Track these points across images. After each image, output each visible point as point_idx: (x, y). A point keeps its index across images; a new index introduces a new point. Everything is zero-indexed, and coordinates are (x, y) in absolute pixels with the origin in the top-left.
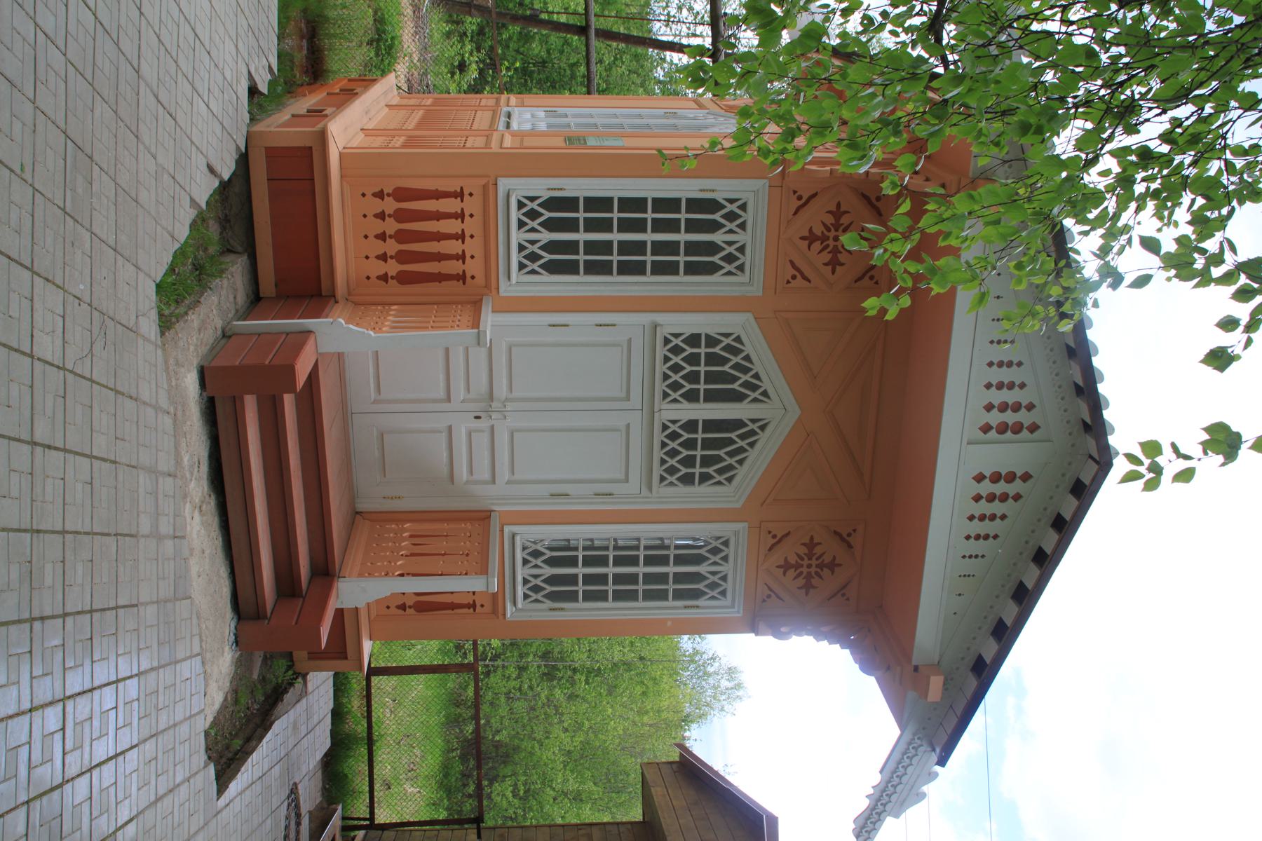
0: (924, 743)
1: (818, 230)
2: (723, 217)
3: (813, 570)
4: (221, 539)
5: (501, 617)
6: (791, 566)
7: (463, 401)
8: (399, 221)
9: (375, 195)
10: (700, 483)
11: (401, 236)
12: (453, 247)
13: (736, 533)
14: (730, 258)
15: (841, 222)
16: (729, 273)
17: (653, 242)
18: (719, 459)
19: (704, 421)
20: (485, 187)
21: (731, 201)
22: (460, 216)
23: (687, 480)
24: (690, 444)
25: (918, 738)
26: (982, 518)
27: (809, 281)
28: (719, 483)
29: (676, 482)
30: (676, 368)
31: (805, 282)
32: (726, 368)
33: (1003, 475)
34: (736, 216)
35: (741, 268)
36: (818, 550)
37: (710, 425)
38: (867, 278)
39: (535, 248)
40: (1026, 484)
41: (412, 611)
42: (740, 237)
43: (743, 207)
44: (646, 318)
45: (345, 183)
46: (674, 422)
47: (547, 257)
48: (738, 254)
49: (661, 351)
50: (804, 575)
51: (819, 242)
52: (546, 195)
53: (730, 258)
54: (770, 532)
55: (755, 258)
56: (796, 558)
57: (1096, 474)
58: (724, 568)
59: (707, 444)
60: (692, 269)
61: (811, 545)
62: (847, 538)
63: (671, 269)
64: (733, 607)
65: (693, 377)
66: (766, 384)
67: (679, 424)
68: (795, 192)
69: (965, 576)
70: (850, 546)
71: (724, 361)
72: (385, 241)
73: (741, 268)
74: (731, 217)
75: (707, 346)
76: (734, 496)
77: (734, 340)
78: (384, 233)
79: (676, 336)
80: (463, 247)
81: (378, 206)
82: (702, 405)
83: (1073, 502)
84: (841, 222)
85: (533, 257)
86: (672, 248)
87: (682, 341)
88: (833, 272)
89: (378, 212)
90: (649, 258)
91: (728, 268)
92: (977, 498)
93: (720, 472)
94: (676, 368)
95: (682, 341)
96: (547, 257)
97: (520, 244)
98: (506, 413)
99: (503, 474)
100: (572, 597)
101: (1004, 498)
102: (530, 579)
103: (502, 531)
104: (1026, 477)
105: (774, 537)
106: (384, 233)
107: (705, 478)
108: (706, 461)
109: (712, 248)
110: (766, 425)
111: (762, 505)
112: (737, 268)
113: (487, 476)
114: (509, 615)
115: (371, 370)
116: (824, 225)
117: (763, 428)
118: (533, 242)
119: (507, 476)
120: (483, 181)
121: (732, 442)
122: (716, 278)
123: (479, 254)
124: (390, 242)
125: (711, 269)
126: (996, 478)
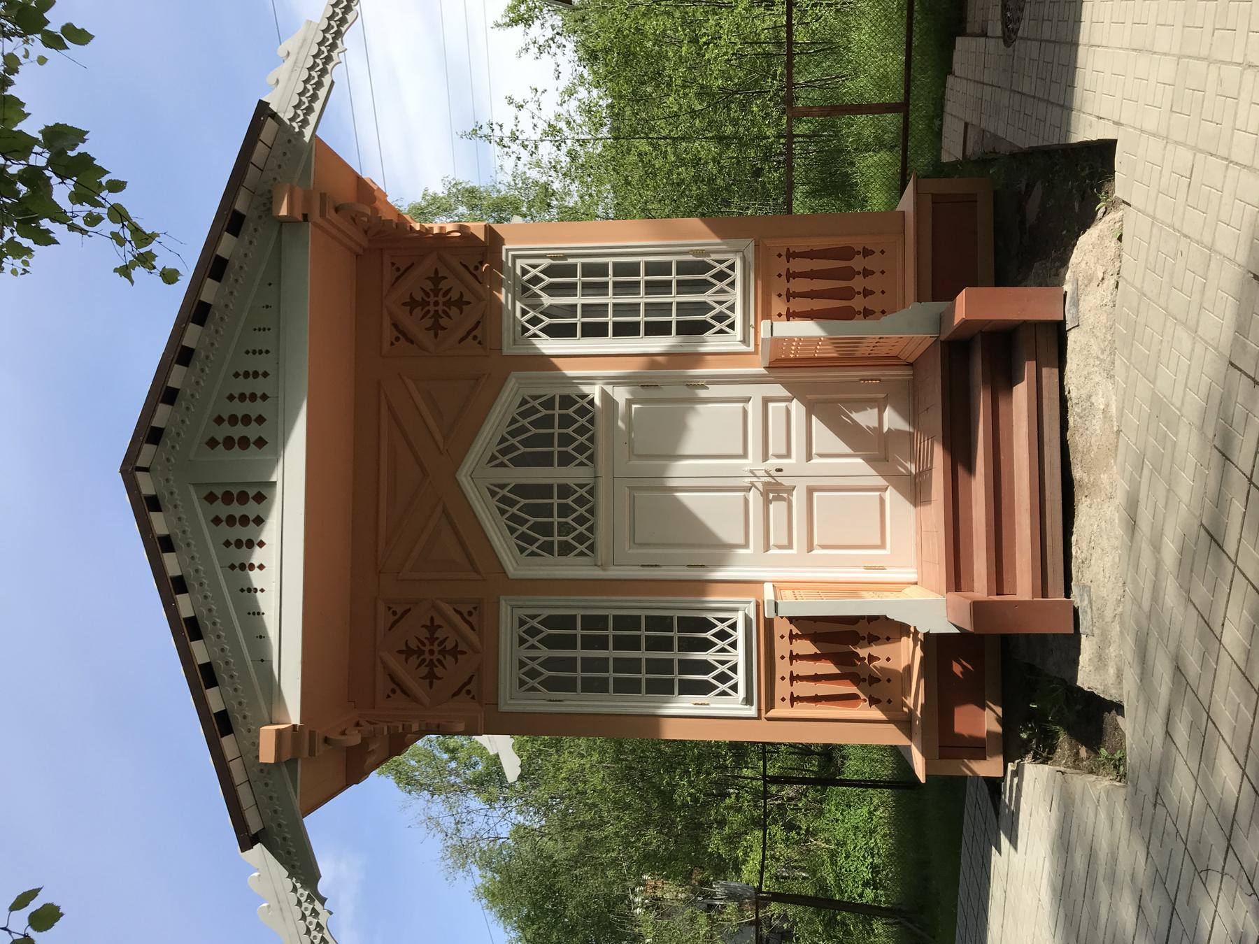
0: (288, 122)
3: (432, 300)
4: (1076, 499)
10: (553, 398)
15: (427, 669)
16: (533, 617)
17: (615, 659)
19: (552, 465)
21: (533, 689)
26: (253, 397)
27: (455, 610)
28: (535, 398)
29: (538, 644)
30: (581, 520)
31: (460, 609)
32: (532, 520)
33: (238, 523)
34: (727, 636)
37: (545, 460)
38: (470, 619)
39: (720, 644)
40: (211, 436)
42: (524, 653)
43: (522, 683)
48: (525, 636)
50: (441, 658)
51: (453, 299)
53: (533, 632)
57: (182, 336)
59: (548, 441)
60: (569, 621)
62: (399, 335)
63: (590, 622)
67: (577, 462)
69: (264, 329)
74: (533, 674)
75: (552, 542)
80: (789, 305)
82: (555, 482)
83: (223, 250)
84: (427, 669)
92: (260, 420)
93: (534, 410)
95: (577, 458)
99: (753, 409)
100: (683, 268)
101: (233, 420)
104: (212, 443)
105: (475, 338)
107: (549, 404)
108: (547, 422)
109: (550, 642)
110: (490, 461)
112: (526, 623)
116: (419, 666)
117: (493, 458)
119: (750, 406)
120: (772, 713)
121: (525, 443)
122: (546, 613)
124: (859, 268)
125: (550, 622)
126: (244, 443)
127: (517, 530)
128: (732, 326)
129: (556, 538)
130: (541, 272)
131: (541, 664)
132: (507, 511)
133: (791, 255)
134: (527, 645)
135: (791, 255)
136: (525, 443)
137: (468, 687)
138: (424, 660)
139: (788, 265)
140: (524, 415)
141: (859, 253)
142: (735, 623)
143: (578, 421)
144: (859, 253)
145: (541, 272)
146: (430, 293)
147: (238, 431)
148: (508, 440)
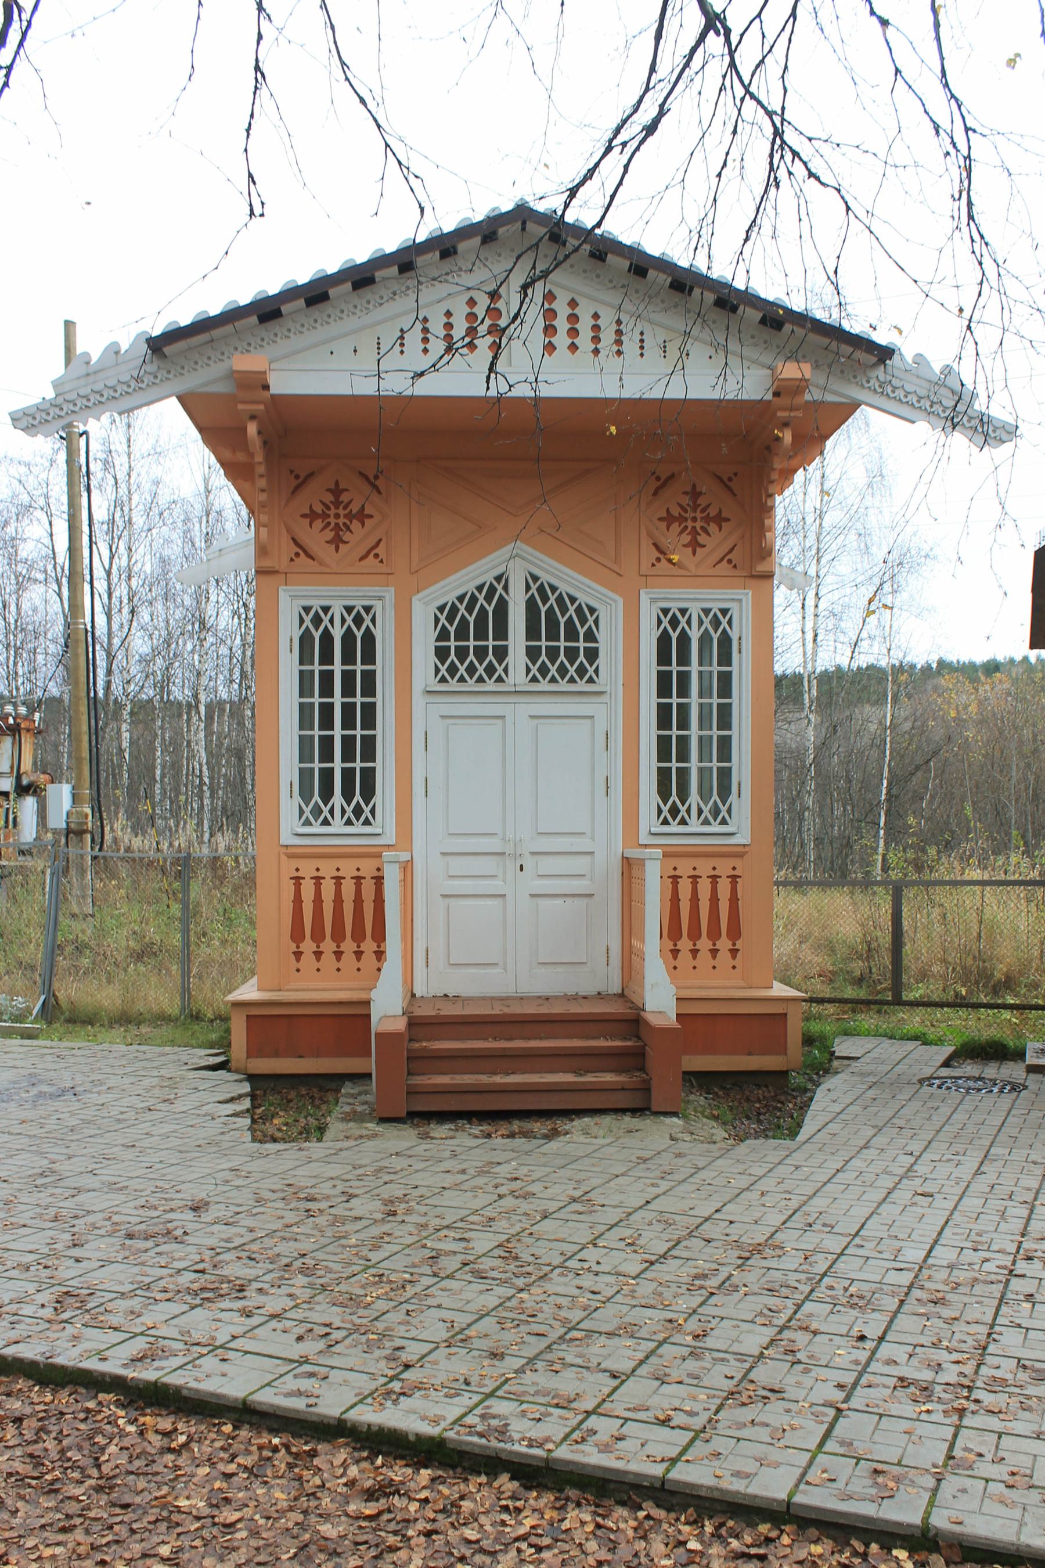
1: (329, 534)
2: (359, 629)
3: (341, 512)
5: (747, 849)
6: (337, 535)
7: (505, 881)
8: (324, 938)
9: (298, 960)
10: (597, 642)
11: (338, 936)
12: (704, 888)
13: (653, 600)
14: (358, 621)
15: (677, 515)
18: (570, 622)
20: (290, 856)
21: (302, 621)
22: (695, 879)
23: (592, 655)
24: (553, 654)
25: (868, 382)
27: (380, 540)
30: (471, 670)
35: (368, 609)
36: (676, 511)
37: (532, 632)
39: (349, 810)
41: (739, 945)
42: (337, 611)
43: (307, 609)
44: (418, 700)
45: (287, 987)
46: (528, 670)
47: (357, 798)
49: (453, 685)
50: (706, 525)
52: (297, 799)
53: (358, 621)
54: (653, 565)
55: (358, 595)
56: (327, 530)
58: (695, 611)
59: (553, 635)
60: (369, 657)
61: (312, 516)
63: (369, 679)
64: (740, 600)
65: (481, 653)
66: (489, 578)
68: (292, 560)
70: (672, 476)
71: (464, 621)
72: (302, 953)
73: (368, 609)
74: (317, 621)
76: (615, 601)
77: (442, 613)
78: (730, 950)
79: (437, 670)
80: (368, 878)
81: (308, 957)
82: (510, 643)
84: (677, 515)
85: (358, 811)
86: (348, 678)
87: (443, 665)
88: (371, 516)
89: (730, 955)
90: (359, 700)
91: (367, 622)
92: (573, 347)
93: (583, 621)
94: (471, 670)
95: (443, 665)
96: (357, 798)
97: (345, 824)
98: (518, 839)
101: (573, 318)
102: (304, 818)
103: (646, 846)
106: (730, 950)
107: (590, 636)
108: (572, 634)
109: (348, 638)
111: (621, 575)
113: (587, 859)
114: (745, 842)
115: (472, 970)
116: (681, 532)
117: (535, 579)
118: (343, 812)
120: (284, 858)
121: (550, 611)
122: (377, 633)
123: (314, 863)
125: (369, 639)
127: (461, 603)
128: (665, 822)
129: (581, 644)
130: (326, 627)
131: (326, 628)
132: (480, 593)
133: (734, 879)
134: (686, 817)
135: (734, 879)
136: (550, 611)
137: (376, 551)
138: (345, 508)
139: (328, 878)
140: (579, 610)
141: (338, 946)
142: (330, 824)
143: (481, 665)
144: (338, 946)
145: (326, 627)
146: (706, 513)
147: (562, 324)
148: (553, 594)
